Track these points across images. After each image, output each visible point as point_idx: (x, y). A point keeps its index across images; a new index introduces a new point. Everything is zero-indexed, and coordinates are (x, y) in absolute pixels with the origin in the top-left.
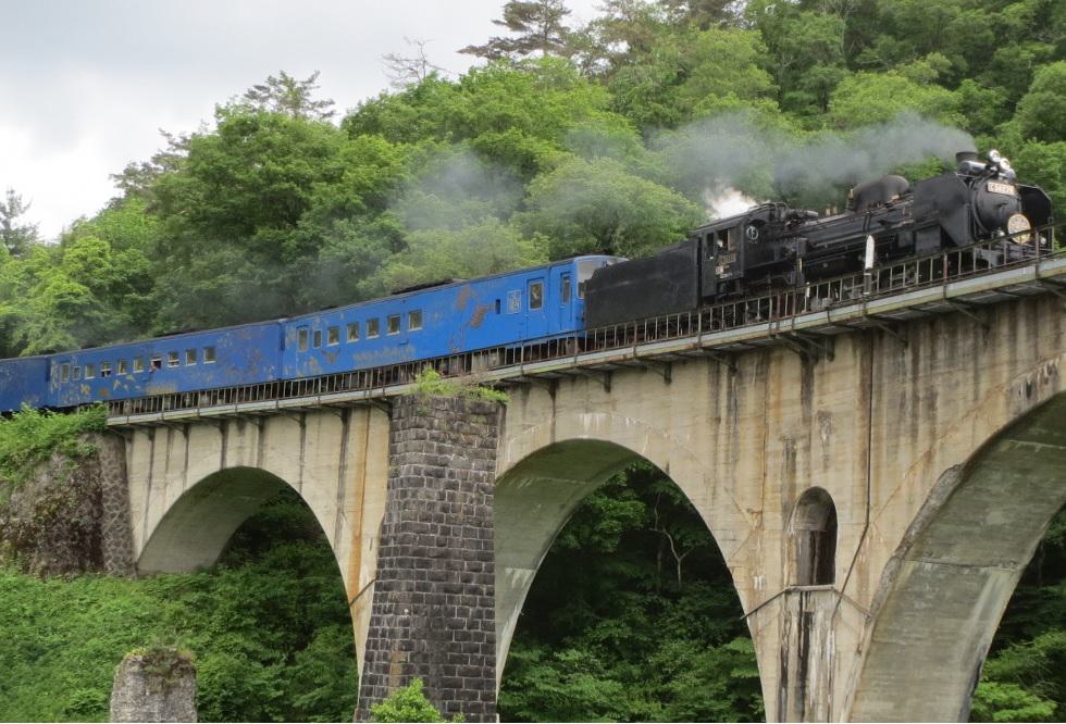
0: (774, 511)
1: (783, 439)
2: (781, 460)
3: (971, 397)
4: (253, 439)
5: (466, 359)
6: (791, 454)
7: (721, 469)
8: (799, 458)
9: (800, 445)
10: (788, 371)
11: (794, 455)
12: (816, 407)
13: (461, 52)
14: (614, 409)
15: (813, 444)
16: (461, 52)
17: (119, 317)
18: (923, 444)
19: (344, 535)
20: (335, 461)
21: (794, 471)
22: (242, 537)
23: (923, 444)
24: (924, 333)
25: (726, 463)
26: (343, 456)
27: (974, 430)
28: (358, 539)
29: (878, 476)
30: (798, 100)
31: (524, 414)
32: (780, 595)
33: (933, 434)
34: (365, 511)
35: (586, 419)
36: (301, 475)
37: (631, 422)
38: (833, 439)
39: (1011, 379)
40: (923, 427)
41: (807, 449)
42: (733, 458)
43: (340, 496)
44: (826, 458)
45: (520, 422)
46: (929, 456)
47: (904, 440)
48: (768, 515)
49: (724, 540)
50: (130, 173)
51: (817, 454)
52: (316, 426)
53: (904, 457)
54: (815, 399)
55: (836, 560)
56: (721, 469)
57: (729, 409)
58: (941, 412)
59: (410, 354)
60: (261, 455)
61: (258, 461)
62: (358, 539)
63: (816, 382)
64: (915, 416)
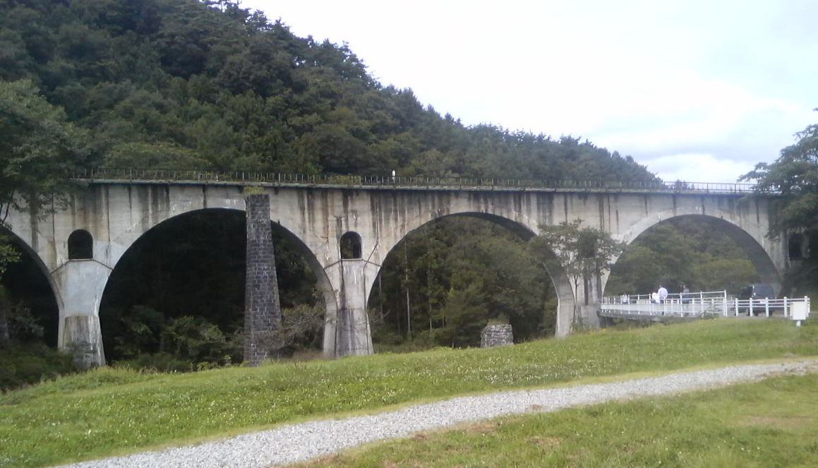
0: (333, 237)
2: (335, 223)
7: (307, 224)
10: (337, 202)
12: (350, 208)
17: (261, 284)
22: (82, 200)
23: (400, 222)
24: (430, 197)
25: (309, 222)
28: (53, 244)
30: (29, 161)
32: (338, 262)
33: (404, 221)
35: (228, 201)
42: (312, 220)
46: (403, 226)
48: (330, 239)
49: (311, 245)
50: (782, 150)
56: (307, 224)
57: (309, 206)
59: (700, 323)
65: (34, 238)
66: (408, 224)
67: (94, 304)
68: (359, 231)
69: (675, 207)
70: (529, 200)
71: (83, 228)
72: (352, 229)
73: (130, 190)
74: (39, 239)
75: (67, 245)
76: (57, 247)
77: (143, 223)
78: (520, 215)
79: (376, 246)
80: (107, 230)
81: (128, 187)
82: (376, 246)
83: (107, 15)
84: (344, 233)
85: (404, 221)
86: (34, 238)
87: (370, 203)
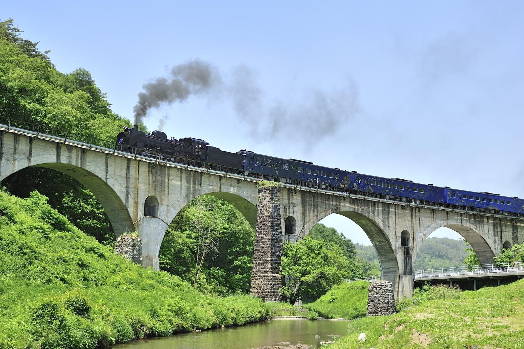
1: (283, 205)
2: (283, 209)
3: (325, 208)
4: (77, 156)
5: (503, 212)
6: (285, 208)
8: (287, 210)
9: (287, 207)
11: (286, 209)
13: (50, 51)
14: (240, 189)
15: (290, 208)
16: (50, 51)
18: (316, 214)
19: (129, 200)
20: (124, 174)
21: (286, 212)
26: (128, 173)
27: (462, 223)
28: (136, 203)
29: (306, 217)
31: (209, 182)
33: (318, 212)
34: (139, 194)
35: (232, 189)
36: (106, 176)
37: (245, 193)
38: (295, 208)
39: (332, 207)
40: (315, 211)
41: (289, 209)
43: (127, 187)
44: (294, 211)
45: (208, 183)
47: (312, 212)
51: (291, 210)
52: (114, 160)
53: (312, 215)
54: (291, 200)
55: (364, 232)
58: (319, 209)
60: (82, 163)
61: (81, 165)
62: (136, 203)
63: (291, 197)
64: (314, 208)
65: (127, 198)
66: (319, 215)
67: (156, 249)
68: (295, 216)
69: (448, 220)
70: (378, 205)
71: (153, 195)
72: (291, 215)
73: (181, 173)
74: (129, 199)
75: (144, 205)
76: (139, 206)
77: (187, 196)
78: (374, 216)
79: (303, 227)
80: (166, 198)
81: (470, 216)
82: (303, 227)
83: (25, 146)
84: (287, 216)
85: (318, 212)
86: (127, 198)
87: (126, 164)
